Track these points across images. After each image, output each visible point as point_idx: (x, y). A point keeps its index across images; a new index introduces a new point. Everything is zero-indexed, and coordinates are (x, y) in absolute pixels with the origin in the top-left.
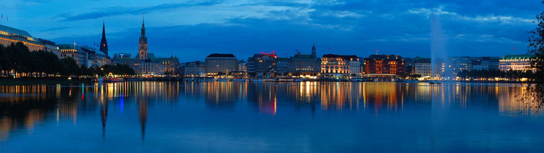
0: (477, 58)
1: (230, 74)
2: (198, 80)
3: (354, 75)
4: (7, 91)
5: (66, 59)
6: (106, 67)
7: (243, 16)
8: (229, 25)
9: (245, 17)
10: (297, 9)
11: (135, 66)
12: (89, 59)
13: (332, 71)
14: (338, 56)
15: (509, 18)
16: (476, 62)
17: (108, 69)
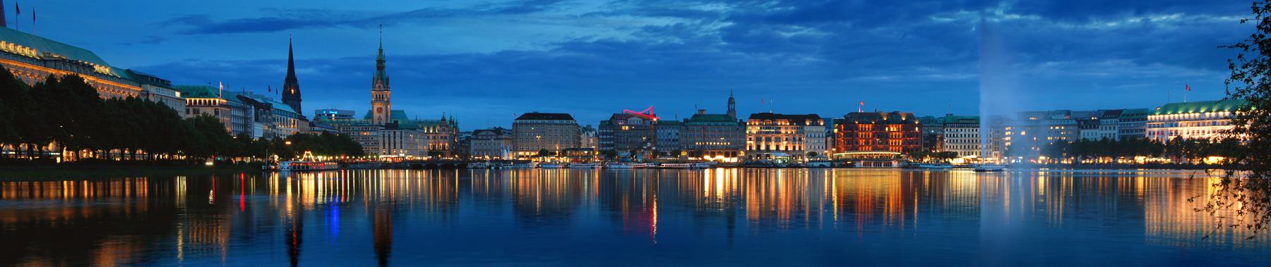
0: (1091, 114)
1: (563, 153)
2: (499, 165)
3: (813, 154)
4: (37, 193)
5: (198, 119)
6: (296, 138)
7: (590, 37)
8: (560, 54)
9: (595, 39)
10: (698, 22)
11: (365, 138)
12: (257, 120)
13: (768, 147)
14: (781, 117)
15: (1174, 17)
16: (1086, 122)
17: (302, 143)
